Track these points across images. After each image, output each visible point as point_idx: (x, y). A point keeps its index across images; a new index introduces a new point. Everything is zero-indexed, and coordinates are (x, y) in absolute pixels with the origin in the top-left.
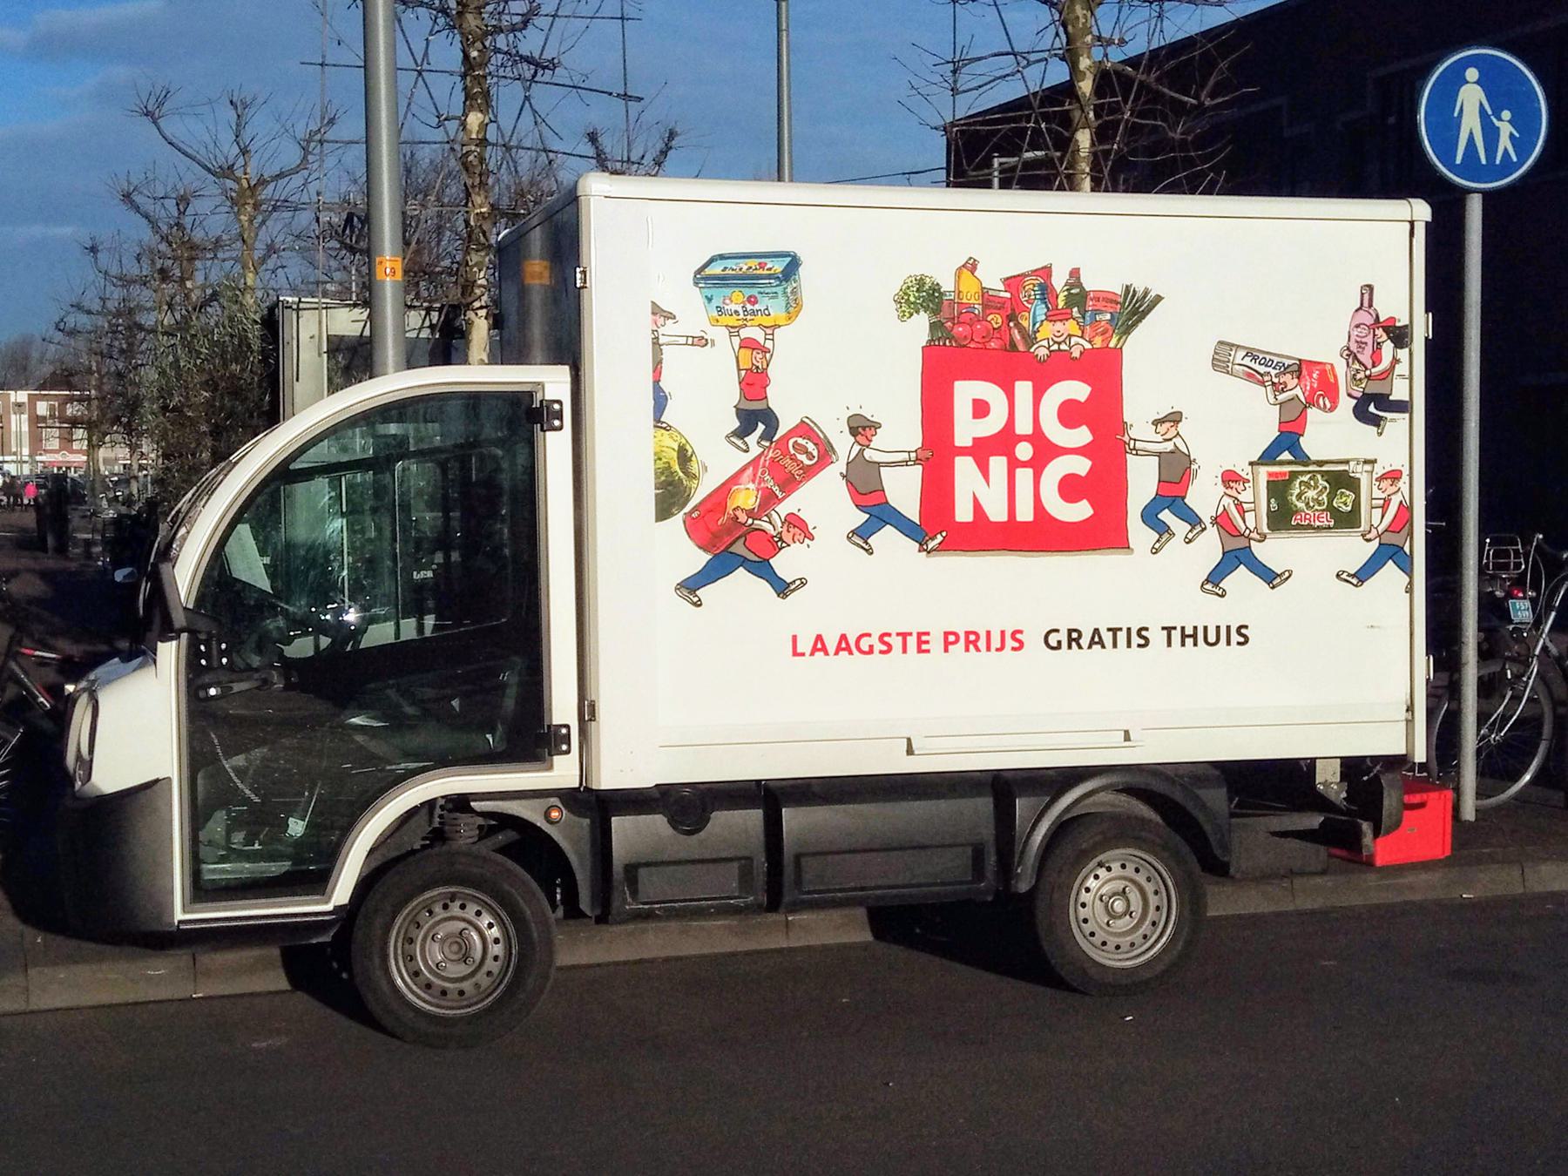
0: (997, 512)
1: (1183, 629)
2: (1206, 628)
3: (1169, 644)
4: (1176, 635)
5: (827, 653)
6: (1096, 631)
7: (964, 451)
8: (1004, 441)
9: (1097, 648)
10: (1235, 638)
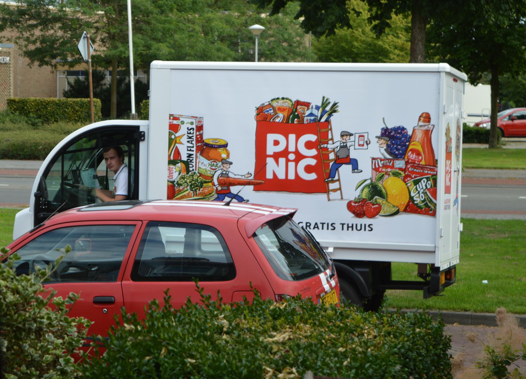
0: (281, 176)
1: (348, 224)
2: (356, 225)
3: (343, 229)
4: (345, 227)
5: (318, 229)
6: (316, 224)
7: (270, 156)
8: (285, 153)
9: (316, 229)
10: (367, 228)
